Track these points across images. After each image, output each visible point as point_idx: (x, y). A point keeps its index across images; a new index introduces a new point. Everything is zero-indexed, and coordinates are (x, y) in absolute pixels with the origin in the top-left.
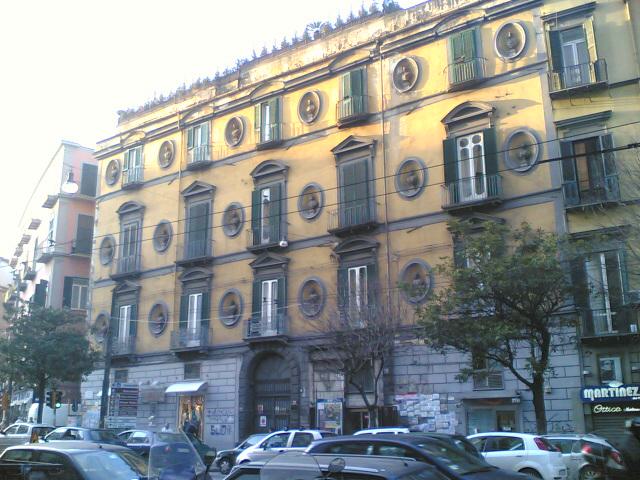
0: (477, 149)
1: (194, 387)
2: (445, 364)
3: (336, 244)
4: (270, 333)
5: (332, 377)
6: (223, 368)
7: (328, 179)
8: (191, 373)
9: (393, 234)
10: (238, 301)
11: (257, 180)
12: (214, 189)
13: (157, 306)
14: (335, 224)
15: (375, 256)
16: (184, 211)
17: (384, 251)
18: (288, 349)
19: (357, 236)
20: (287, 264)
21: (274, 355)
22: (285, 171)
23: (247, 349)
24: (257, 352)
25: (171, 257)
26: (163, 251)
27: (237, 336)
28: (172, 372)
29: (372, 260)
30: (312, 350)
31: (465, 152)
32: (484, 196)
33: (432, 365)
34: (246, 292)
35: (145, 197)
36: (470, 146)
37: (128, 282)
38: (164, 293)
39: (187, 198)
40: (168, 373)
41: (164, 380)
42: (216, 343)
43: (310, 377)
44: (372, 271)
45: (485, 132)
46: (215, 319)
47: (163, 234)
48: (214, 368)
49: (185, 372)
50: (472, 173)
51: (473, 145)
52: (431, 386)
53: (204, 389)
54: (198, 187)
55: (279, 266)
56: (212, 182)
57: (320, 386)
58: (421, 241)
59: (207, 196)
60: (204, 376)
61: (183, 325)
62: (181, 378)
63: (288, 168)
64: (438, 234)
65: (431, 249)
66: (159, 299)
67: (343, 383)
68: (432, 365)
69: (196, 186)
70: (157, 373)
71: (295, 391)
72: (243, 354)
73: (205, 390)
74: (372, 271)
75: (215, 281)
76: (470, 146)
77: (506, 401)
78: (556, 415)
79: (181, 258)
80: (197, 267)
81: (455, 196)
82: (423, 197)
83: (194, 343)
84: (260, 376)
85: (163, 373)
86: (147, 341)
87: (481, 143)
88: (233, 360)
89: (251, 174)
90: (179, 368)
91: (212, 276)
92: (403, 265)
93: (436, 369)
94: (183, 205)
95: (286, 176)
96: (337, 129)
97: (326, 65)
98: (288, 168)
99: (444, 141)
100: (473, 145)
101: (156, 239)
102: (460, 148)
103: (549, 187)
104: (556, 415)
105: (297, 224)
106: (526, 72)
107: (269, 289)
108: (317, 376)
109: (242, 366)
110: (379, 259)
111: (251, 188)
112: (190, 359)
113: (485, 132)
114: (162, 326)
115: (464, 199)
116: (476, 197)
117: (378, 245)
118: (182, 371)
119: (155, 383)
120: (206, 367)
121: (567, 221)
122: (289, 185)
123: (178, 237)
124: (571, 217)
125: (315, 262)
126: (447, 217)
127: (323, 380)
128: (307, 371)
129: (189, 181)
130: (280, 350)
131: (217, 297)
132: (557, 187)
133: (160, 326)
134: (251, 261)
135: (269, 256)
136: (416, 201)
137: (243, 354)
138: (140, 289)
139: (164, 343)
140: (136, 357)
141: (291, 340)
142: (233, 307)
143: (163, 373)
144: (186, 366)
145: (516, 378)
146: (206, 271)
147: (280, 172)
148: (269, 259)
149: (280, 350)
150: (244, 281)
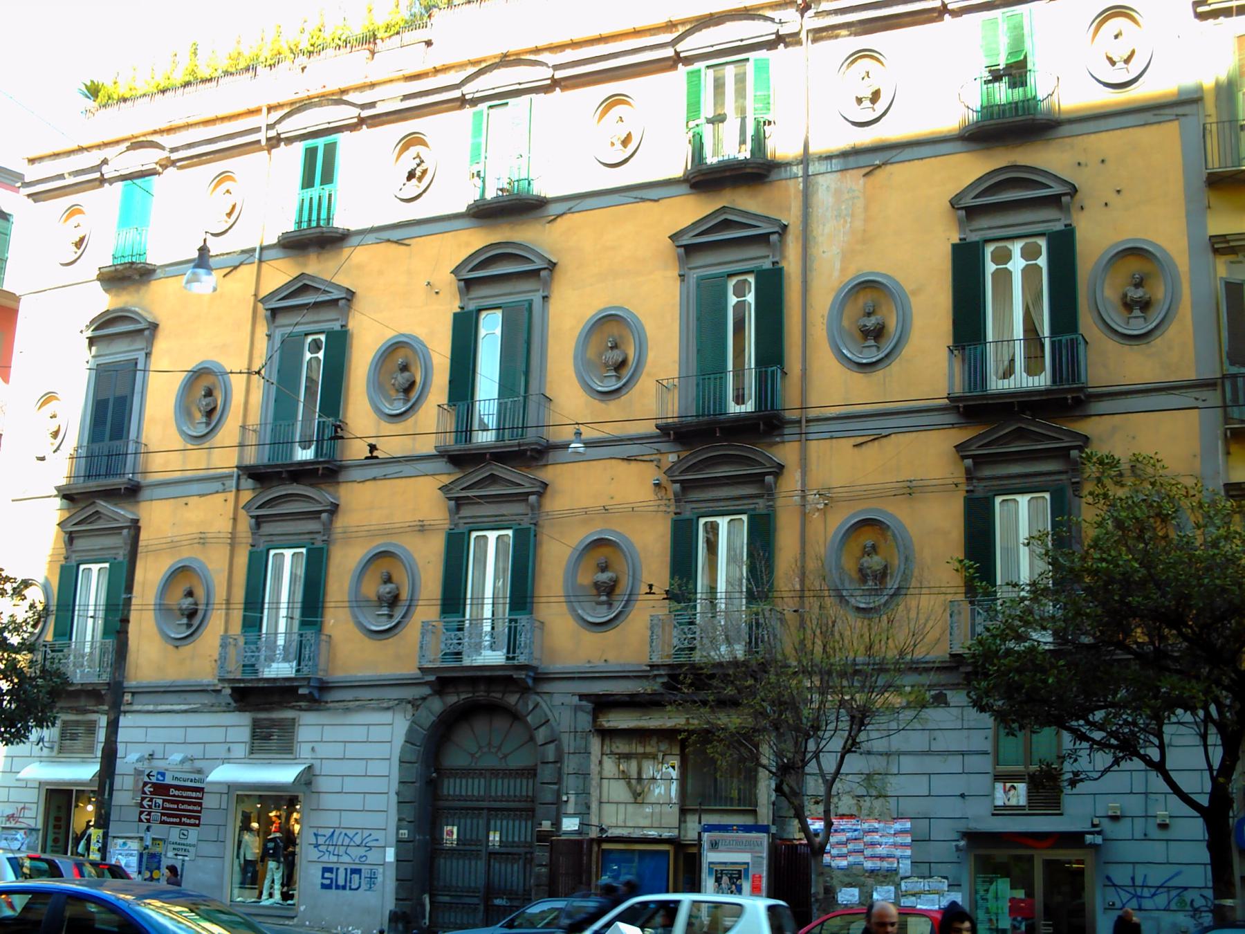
0: (1030, 273)
1: (284, 774)
2: (928, 753)
3: (672, 458)
4: (493, 657)
5: (649, 769)
6: (359, 733)
7: (659, 306)
8: (269, 740)
9: (817, 448)
10: (200, 593)
11: (468, 285)
12: (350, 295)
13: (181, 572)
14: (673, 409)
15: (769, 493)
16: (262, 345)
17: (791, 482)
18: (533, 699)
19: (724, 449)
20: (540, 495)
21: (493, 709)
22: (542, 273)
23: (426, 691)
24: (452, 699)
25: (226, 450)
26: (861, 366)
27: (408, 653)
28: (218, 734)
29: (761, 505)
30: (602, 704)
31: (1004, 277)
32: (1042, 381)
33: (900, 754)
34: (428, 557)
35: (156, 300)
36: (1017, 264)
37: (103, 506)
38: (203, 540)
39: (274, 312)
40: (203, 735)
41: (196, 751)
42: (339, 673)
43: (594, 768)
44: (762, 535)
45: (330, 335)
46: (338, 621)
47: (204, 395)
48: (329, 733)
49: (254, 736)
50: (1018, 331)
51: (1009, 266)
52: (893, 801)
53: (307, 779)
54: (305, 289)
55: (315, 515)
56: (344, 281)
57: (617, 790)
58: (884, 460)
59: (140, 344)
60: (304, 751)
61: (252, 622)
62: (241, 750)
63: (552, 266)
64: (933, 455)
65: (911, 490)
66: (185, 555)
67: (674, 787)
68: (900, 754)
69: (302, 286)
70: (178, 735)
71: (549, 797)
72: (415, 704)
73: (309, 783)
74: (762, 535)
75: (341, 522)
76: (1017, 264)
77: (1074, 839)
78: (1177, 874)
79: (252, 457)
80: (291, 485)
81: (976, 372)
82: (895, 367)
83: (281, 669)
84: (456, 758)
85: (193, 735)
86: (351, 649)
87: (1042, 261)
88: (386, 717)
89: (455, 272)
90: (238, 726)
91: (334, 509)
92: (839, 519)
93: (908, 764)
94: (262, 330)
95: (547, 284)
96: (685, 188)
97: (668, 37)
98: (552, 266)
99: (455, 314)
100: (1009, 266)
101: (184, 409)
102: (991, 267)
103: (1191, 375)
104: (1177, 874)
105: (826, 379)
106: (1148, 117)
107: (491, 549)
108: (609, 766)
109: (410, 731)
110: (780, 502)
111: (451, 304)
112: (266, 704)
113: (761, 275)
114: (193, 617)
115: (997, 384)
116: (1022, 381)
117: (779, 470)
118: (245, 734)
119: (177, 757)
120: (311, 729)
121: (1228, 453)
122: (555, 306)
123: (247, 401)
124: (1234, 448)
125: (608, 494)
126: (441, 465)
127: (625, 776)
128: (64, 749)
129: (279, 274)
130: (512, 699)
131: (345, 563)
132: (1207, 375)
133: (191, 619)
134: (446, 480)
135: (498, 471)
136: (878, 375)
137: (415, 704)
138: (544, 488)
139: (204, 658)
140: (324, 687)
141: (541, 678)
142: (389, 587)
143: (193, 735)
144: (256, 725)
145: (1167, 789)
146: (124, 512)
147: (535, 273)
148: (493, 479)
149: (512, 699)
150: (423, 528)
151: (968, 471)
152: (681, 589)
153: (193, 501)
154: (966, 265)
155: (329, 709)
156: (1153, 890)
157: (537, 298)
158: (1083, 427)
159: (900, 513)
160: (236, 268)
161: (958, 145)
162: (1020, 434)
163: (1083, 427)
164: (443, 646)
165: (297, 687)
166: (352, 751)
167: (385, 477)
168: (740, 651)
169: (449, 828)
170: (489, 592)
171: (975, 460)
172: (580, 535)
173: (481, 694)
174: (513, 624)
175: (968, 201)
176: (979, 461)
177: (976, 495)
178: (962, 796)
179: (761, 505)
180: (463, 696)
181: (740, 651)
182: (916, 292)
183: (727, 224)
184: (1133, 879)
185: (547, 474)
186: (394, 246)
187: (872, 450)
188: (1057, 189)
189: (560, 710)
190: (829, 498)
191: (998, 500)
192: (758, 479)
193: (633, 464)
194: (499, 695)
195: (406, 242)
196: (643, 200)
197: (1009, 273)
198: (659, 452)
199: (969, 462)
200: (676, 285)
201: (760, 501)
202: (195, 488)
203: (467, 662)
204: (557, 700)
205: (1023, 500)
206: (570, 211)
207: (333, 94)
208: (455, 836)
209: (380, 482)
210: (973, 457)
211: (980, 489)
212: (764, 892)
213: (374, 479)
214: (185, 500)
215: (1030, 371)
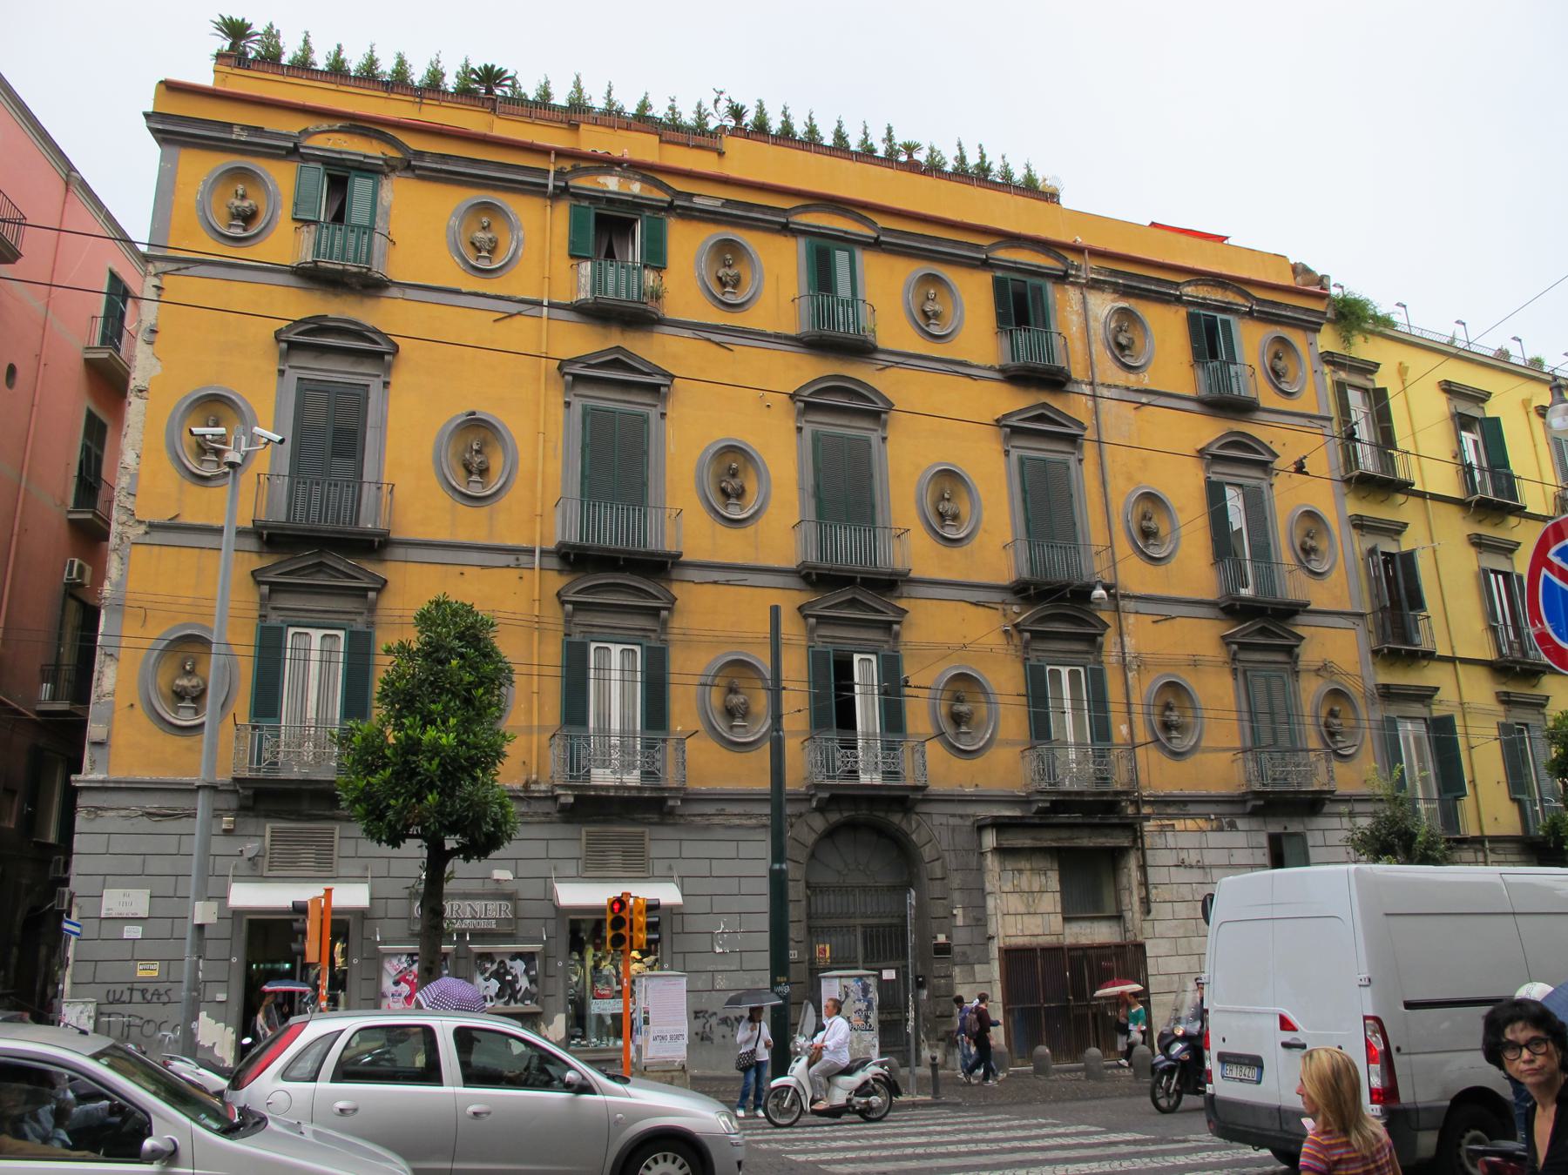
6: (728, 849)
20: (379, 591)
90: (1249, 838)
130: (896, 818)
138: (382, 585)
139: (222, 751)
151: (262, 597)
155: (674, 824)
159: (1187, 679)
160: (511, 316)
161: (291, 280)
162: (853, 603)
164: (658, 756)
165: (665, 799)
166: (719, 868)
167: (727, 583)
170: (1069, 718)
171: (272, 588)
172: (161, 629)
173: (863, 813)
174: (257, 732)
176: (276, 588)
177: (268, 623)
179: (359, 624)
180: (846, 814)
182: (1181, 510)
183: (1040, 418)
185: (676, 589)
188: (383, 348)
189: (934, 833)
191: (291, 631)
192: (361, 593)
193: (981, 610)
194: (882, 814)
199: (266, 589)
200: (560, 411)
201: (359, 619)
202: (475, 557)
203: (282, 776)
204: (937, 820)
207: (586, 169)
210: (271, 584)
211: (274, 619)
212: (884, 1017)
213: (715, 583)
214: (460, 569)
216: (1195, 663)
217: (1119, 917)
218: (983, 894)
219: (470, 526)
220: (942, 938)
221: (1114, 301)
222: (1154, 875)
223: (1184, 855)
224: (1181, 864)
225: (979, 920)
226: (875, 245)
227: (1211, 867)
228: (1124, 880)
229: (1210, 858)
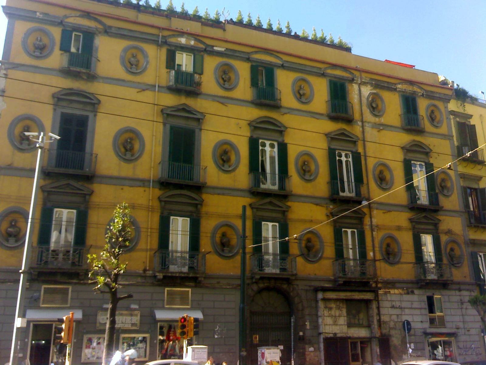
57: (329, 320)
64: (402, 218)
74: (284, 231)
83: (432, 277)
93: (407, 311)
138: (92, 193)
152: (339, 253)
153: (126, 188)
154: (332, 154)
156: (468, 349)
157: (91, 115)
158: (289, 204)
159: (396, 234)
163: (289, 204)
168: (185, 269)
169: (255, 336)
175: (254, 124)
178: (422, 322)
180: (266, 285)
181: (185, 269)
184: (463, 346)
186: (220, 105)
187: (388, 215)
190: (379, 228)
195: (226, 104)
196: (314, 117)
197: (265, 151)
198: (327, 204)
205: (180, 219)
206: (289, 113)
208: (258, 339)
209: (221, 196)
215: (350, 192)
216: (399, 228)
217: (369, 326)
218: (317, 316)
219: (126, 170)
220: (301, 334)
221: (371, 90)
222: (383, 311)
223: (394, 303)
224: (393, 307)
225: (316, 326)
226: (283, 67)
227: (405, 308)
228: (371, 312)
229: (404, 305)
